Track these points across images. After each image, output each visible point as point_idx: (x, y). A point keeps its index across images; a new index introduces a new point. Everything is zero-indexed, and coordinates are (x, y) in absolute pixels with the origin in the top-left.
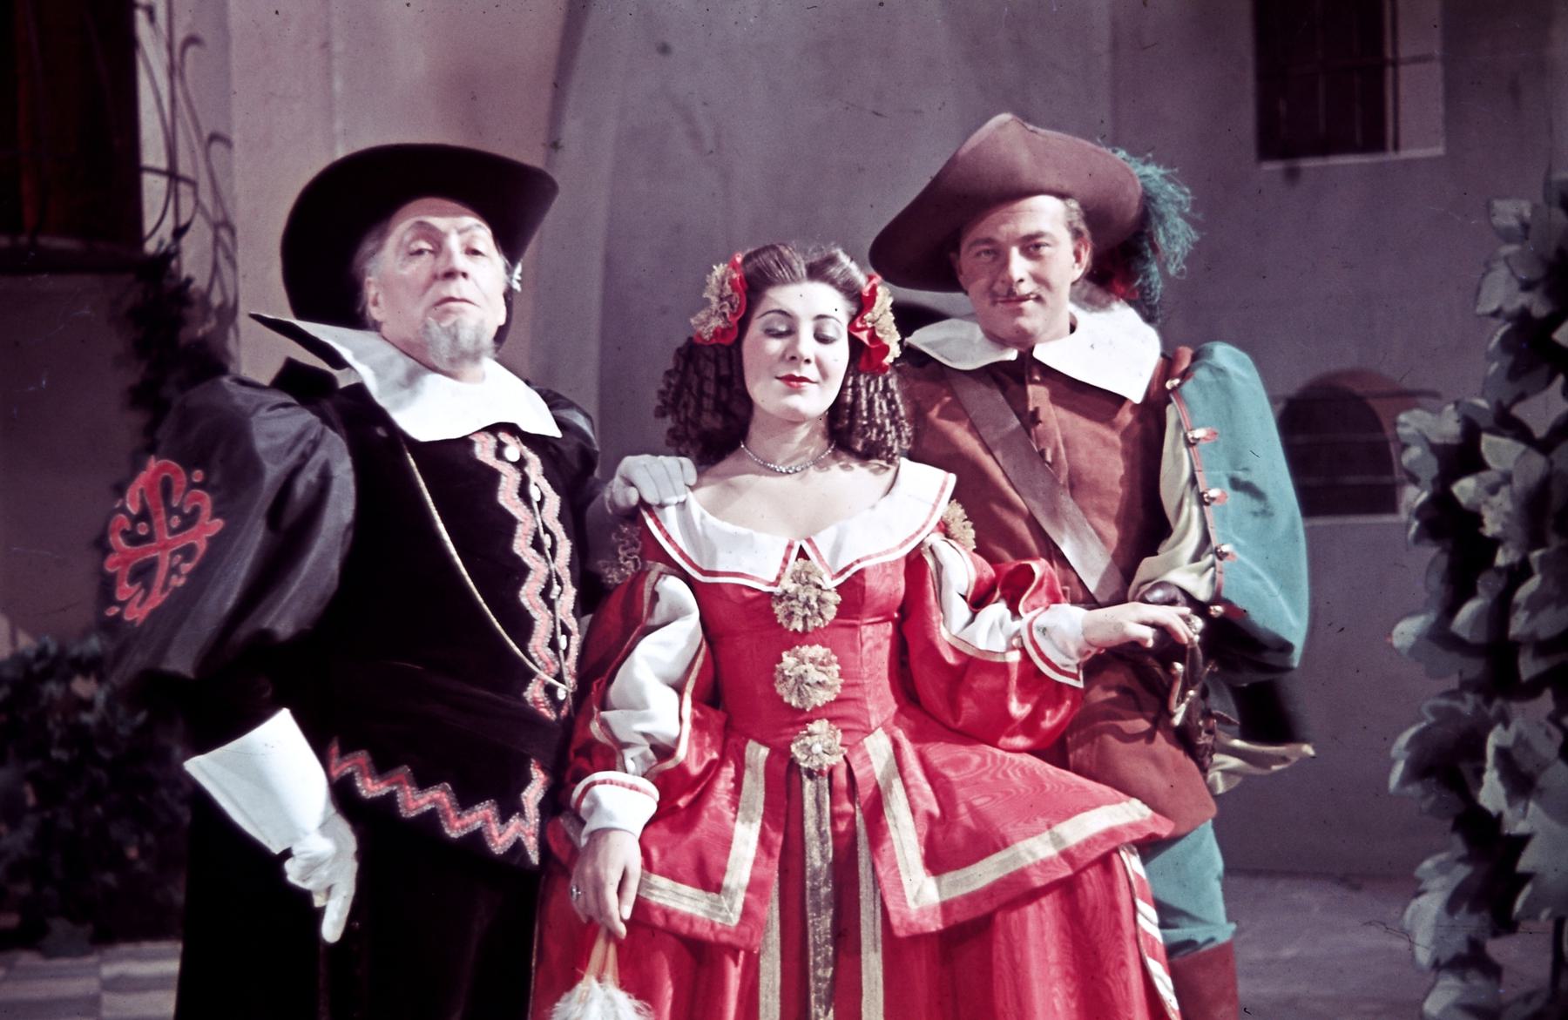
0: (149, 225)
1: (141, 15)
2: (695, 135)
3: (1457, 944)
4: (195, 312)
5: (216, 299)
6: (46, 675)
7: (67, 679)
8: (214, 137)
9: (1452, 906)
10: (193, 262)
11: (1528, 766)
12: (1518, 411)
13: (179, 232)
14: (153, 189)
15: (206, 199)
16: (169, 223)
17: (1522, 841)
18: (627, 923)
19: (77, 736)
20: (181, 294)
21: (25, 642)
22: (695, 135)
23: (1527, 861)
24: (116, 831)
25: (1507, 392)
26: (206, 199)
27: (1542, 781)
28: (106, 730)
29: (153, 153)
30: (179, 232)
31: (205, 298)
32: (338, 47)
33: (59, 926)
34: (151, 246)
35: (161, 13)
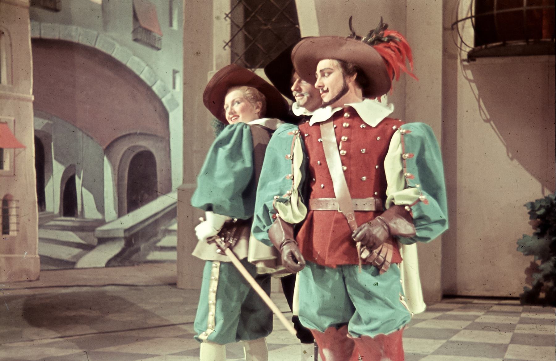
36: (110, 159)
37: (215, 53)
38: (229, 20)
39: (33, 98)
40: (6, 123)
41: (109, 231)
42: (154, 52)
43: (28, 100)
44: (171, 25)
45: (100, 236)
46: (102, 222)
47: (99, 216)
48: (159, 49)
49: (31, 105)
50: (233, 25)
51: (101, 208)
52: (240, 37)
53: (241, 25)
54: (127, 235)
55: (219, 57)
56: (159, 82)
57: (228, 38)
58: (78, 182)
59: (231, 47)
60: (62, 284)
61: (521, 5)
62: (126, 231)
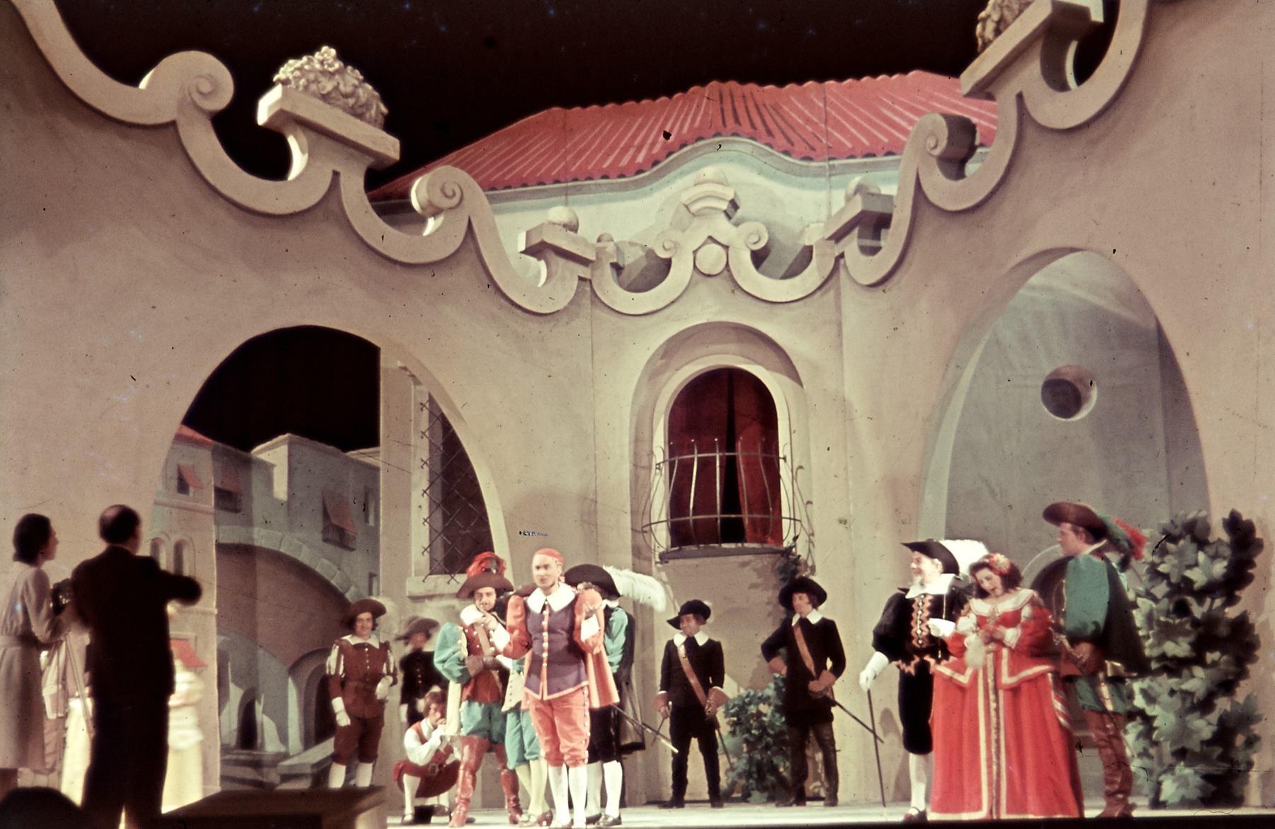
0: (784, 535)
1: (781, 461)
2: (992, 492)
3: (1140, 750)
4: (801, 568)
5: (810, 563)
6: (750, 703)
7: (757, 704)
8: (809, 502)
9: (1138, 737)
10: (801, 550)
11: (1153, 694)
12: (1153, 591)
13: (795, 538)
14: (785, 523)
15: (806, 525)
16: (792, 535)
17: (1154, 718)
18: (390, 125)
19: (763, 727)
20: (797, 561)
21: (743, 692)
22: (992, 492)
23: (1156, 724)
24: (775, 761)
25: (1149, 585)
26: (806, 525)
27: (1160, 699)
28: (772, 724)
29: (785, 512)
30: (795, 538)
31: (806, 563)
32: (850, 468)
33: (756, 795)
34: (785, 544)
35: (789, 459)
36: (295, 681)
37: (413, 560)
38: (426, 468)
39: (216, 611)
40: (186, 640)
41: (291, 767)
42: (346, 553)
43: (211, 614)
44: (367, 521)
45: (285, 772)
46: (286, 756)
47: (283, 749)
48: (352, 550)
49: (213, 621)
50: (432, 530)
51: (284, 738)
52: (439, 543)
53: (440, 530)
54: (315, 770)
55: (417, 563)
56: (353, 589)
57: (426, 544)
58: (259, 708)
59: (430, 552)
60: (867, 706)
61: (715, 512)
62: (314, 766)
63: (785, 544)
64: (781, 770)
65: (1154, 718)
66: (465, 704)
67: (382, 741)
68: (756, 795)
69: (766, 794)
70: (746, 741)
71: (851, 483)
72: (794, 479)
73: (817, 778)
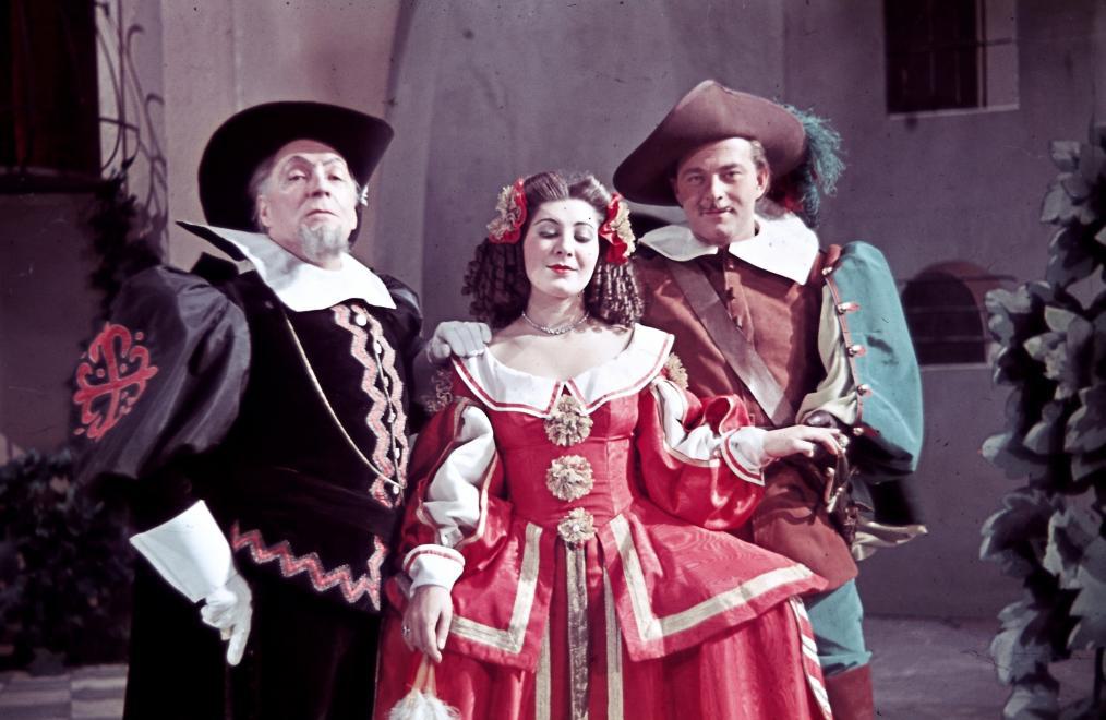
0: (105, 158)
1: (99, 11)
3: (1028, 666)
5: (152, 211)
6: (33, 476)
7: (47, 479)
8: (151, 97)
9: (1024, 640)
11: (1077, 541)
12: (1071, 290)
13: (126, 164)
14: (108, 133)
15: (146, 141)
19: (54, 519)
22: (490, 96)
23: (1076, 609)
24: (82, 587)
26: (146, 141)
29: (108, 108)
30: (126, 164)
31: (145, 210)
32: (239, 33)
34: (106, 174)
35: (113, 9)
63: (106, 174)
64: (94, 602)
65: (1073, 594)
66: (163, 214)
67: (693, 158)
68: (42, 653)
69: (63, 655)
70: (23, 549)
71: (239, 60)
72: (123, 50)
73: (577, 691)
